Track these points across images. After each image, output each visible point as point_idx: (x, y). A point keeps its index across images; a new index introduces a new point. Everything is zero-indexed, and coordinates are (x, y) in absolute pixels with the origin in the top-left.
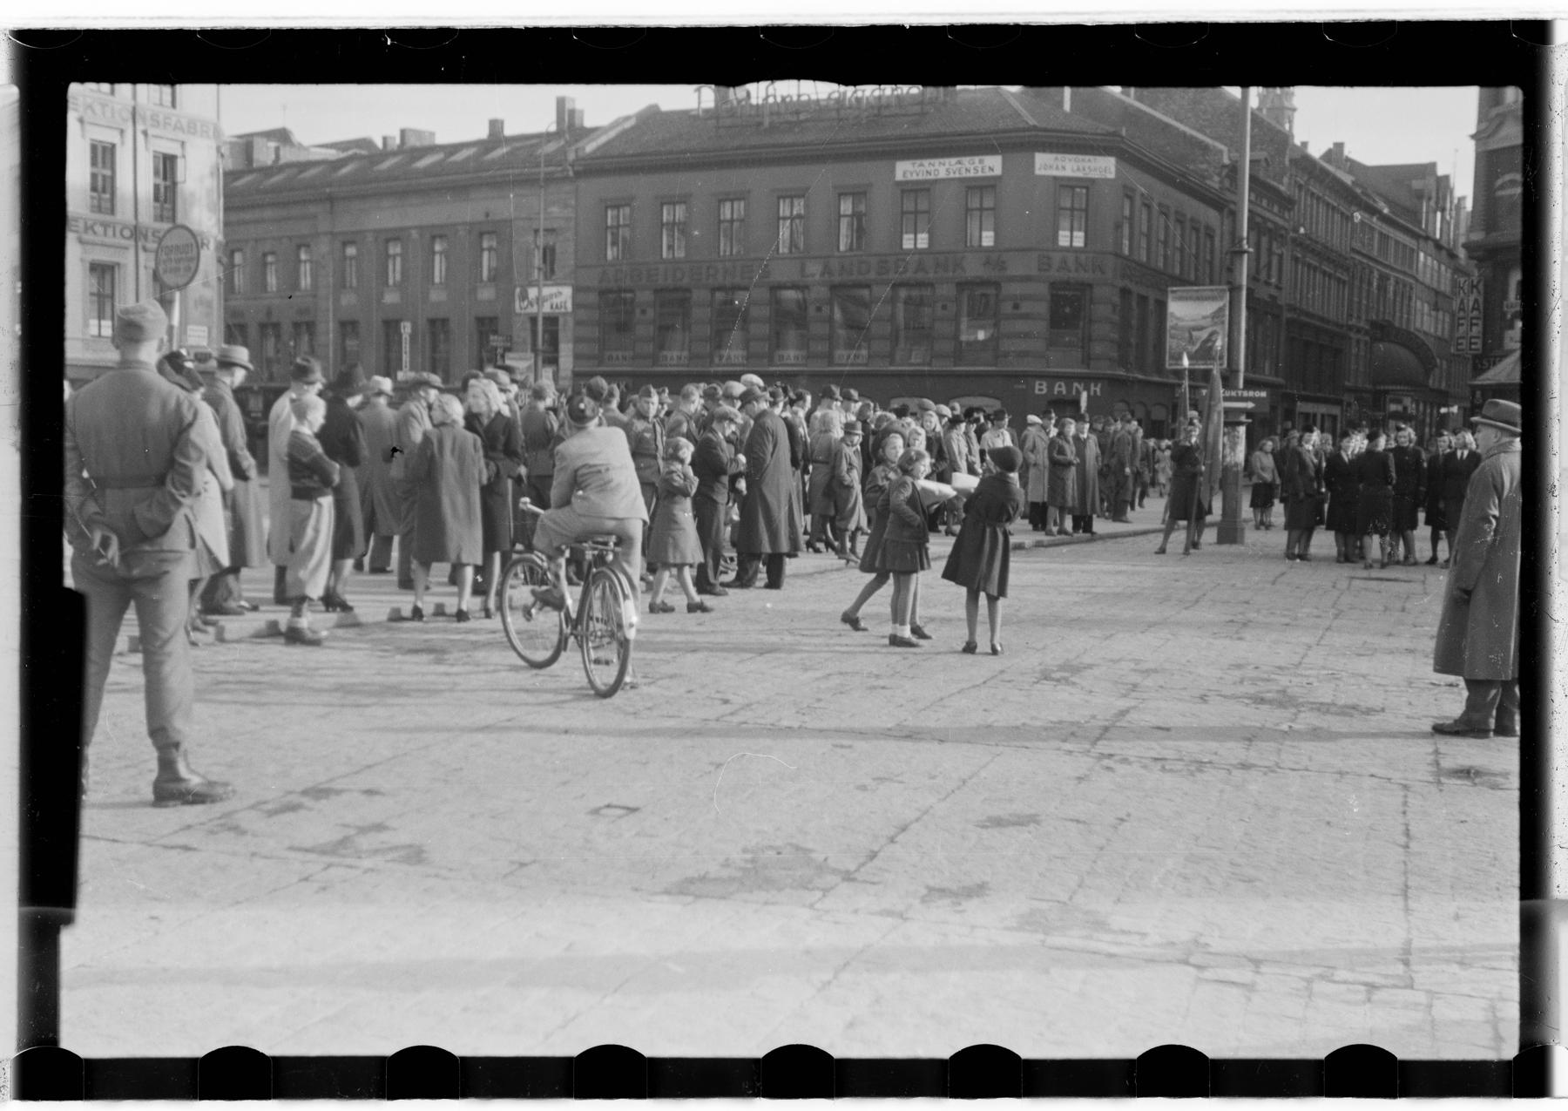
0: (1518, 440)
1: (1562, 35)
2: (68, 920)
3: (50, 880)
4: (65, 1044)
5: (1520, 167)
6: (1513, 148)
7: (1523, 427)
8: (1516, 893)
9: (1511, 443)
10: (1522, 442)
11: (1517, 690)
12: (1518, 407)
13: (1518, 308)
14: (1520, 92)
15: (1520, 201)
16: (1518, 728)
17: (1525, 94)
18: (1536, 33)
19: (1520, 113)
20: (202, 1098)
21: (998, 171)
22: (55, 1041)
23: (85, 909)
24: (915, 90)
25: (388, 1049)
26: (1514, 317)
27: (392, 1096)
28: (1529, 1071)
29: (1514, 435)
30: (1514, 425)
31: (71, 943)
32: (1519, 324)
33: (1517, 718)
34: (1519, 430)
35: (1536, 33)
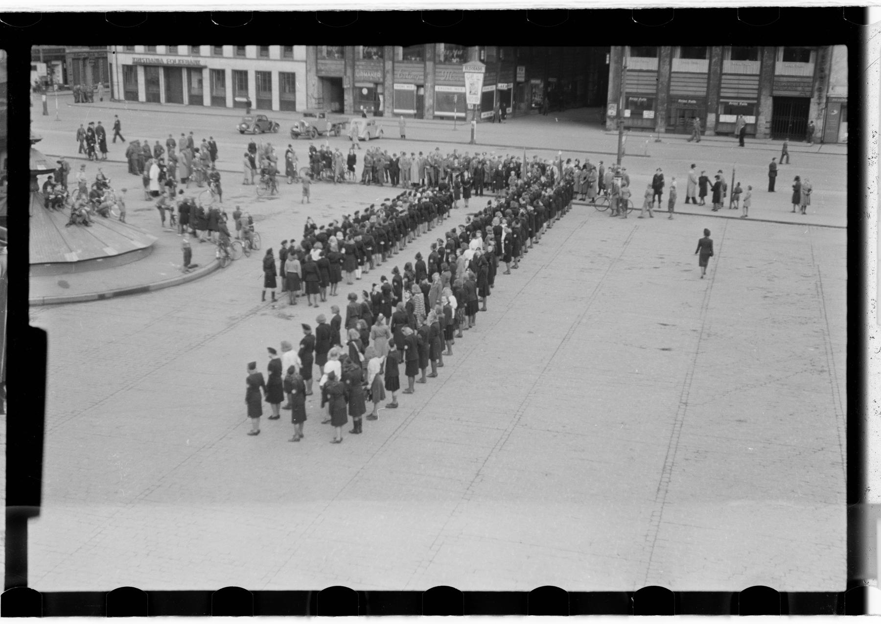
0: (6, 248)
1: (874, 18)
2: (36, 514)
3: (26, 493)
4: (31, 585)
5: (6, 95)
6: (2, 84)
7: (8, 241)
8: (4, 502)
9: (2, 249)
10: (8, 249)
11: (5, 388)
12: (5, 229)
13: (5, 174)
14: (5, 53)
15: (6, 114)
16: (5, 409)
17: (8, 54)
18: (859, 15)
19: (5, 65)
20: (214, 615)
21: (832, 93)
22: (26, 584)
23: (46, 507)
24: (86, 49)
25: (215, 586)
26: (3, 179)
27: (110, 615)
28: (853, 600)
29: (3, 245)
30: (4, 239)
31: (34, 527)
32: (6, 183)
33: (5, 404)
34: (6, 242)
35: (859, 15)
